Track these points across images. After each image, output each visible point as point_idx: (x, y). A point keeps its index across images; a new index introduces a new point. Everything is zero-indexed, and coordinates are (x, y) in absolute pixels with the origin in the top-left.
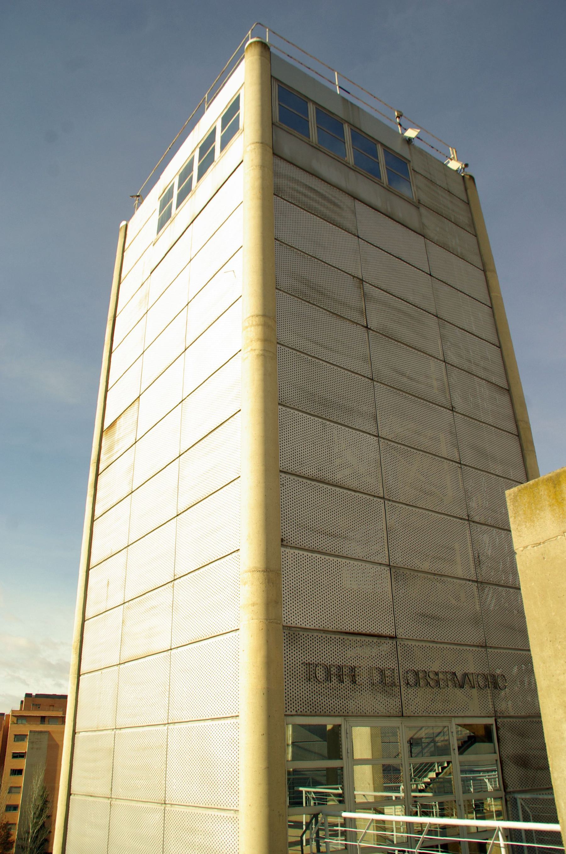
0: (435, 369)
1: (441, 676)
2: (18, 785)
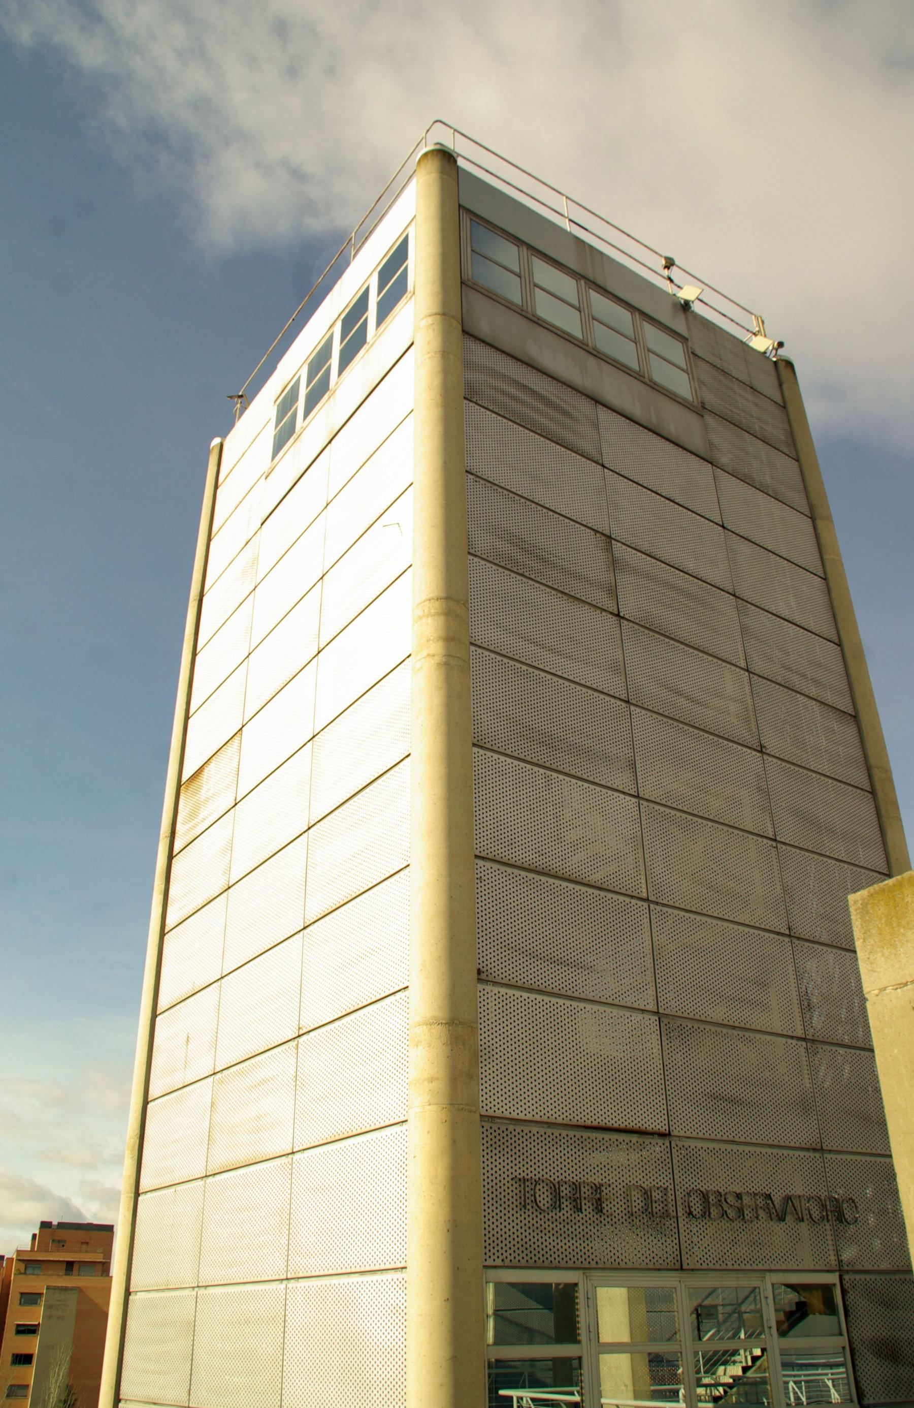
0: (732, 683)
1: (746, 1200)
2: (24, 1383)
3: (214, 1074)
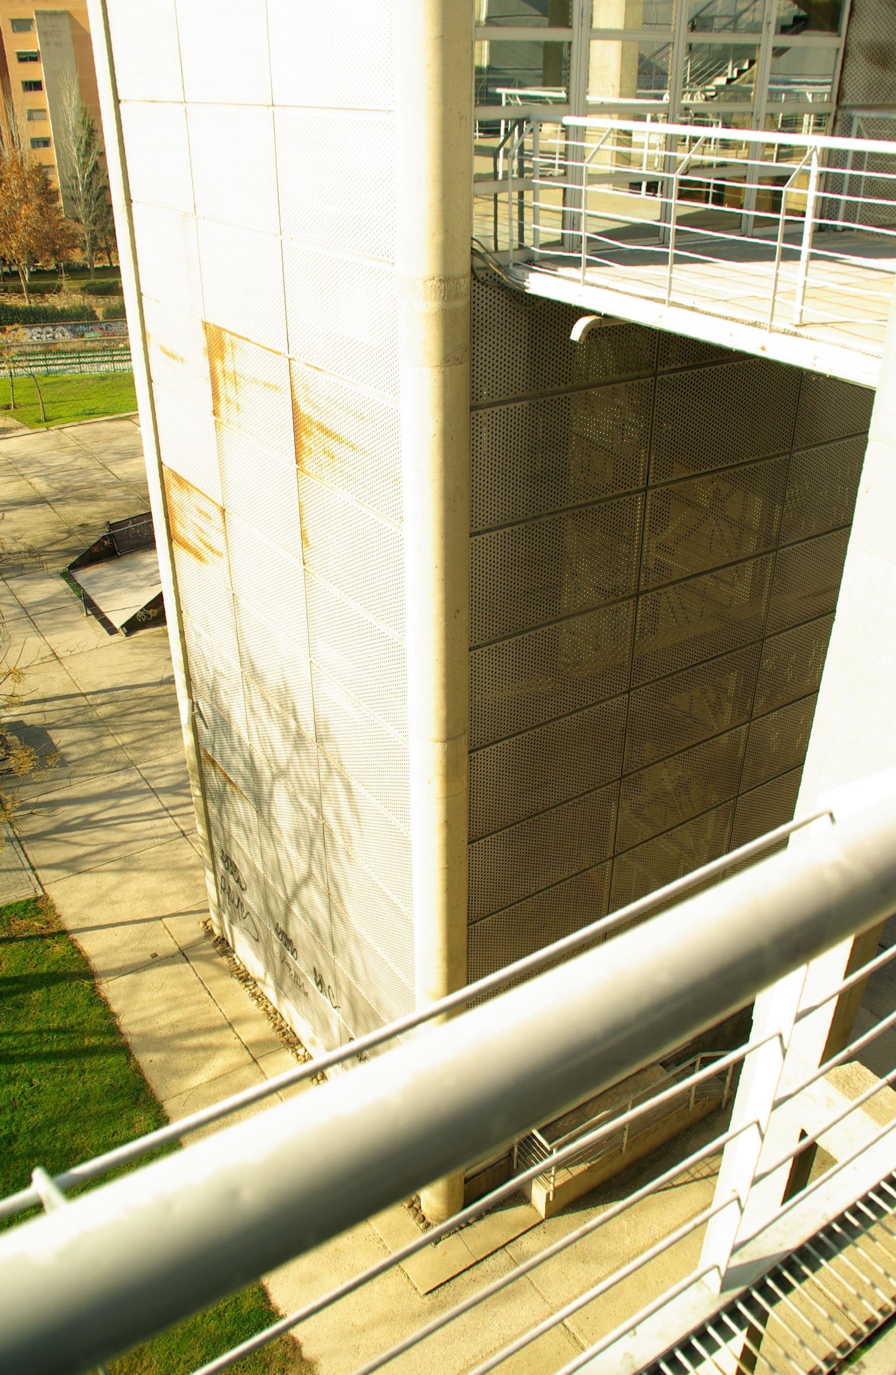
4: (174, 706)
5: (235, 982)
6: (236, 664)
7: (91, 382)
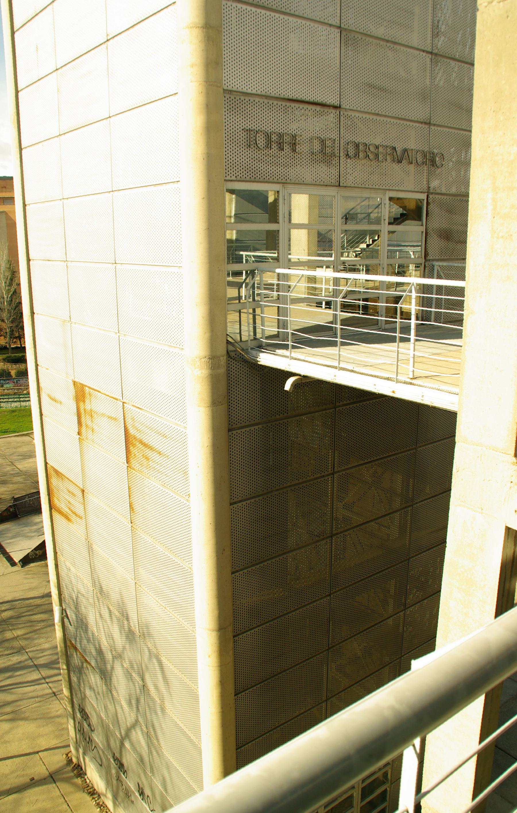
1: (381, 150)
3: (57, 70)
4: (51, 611)
5: (88, 798)
6: (90, 585)
7: (6, 414)
